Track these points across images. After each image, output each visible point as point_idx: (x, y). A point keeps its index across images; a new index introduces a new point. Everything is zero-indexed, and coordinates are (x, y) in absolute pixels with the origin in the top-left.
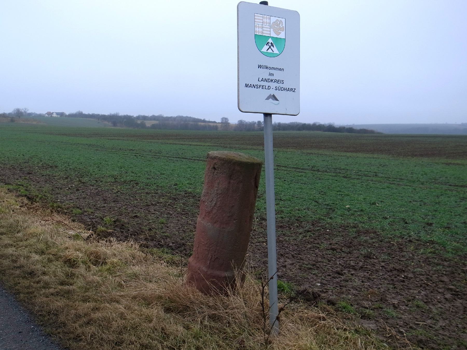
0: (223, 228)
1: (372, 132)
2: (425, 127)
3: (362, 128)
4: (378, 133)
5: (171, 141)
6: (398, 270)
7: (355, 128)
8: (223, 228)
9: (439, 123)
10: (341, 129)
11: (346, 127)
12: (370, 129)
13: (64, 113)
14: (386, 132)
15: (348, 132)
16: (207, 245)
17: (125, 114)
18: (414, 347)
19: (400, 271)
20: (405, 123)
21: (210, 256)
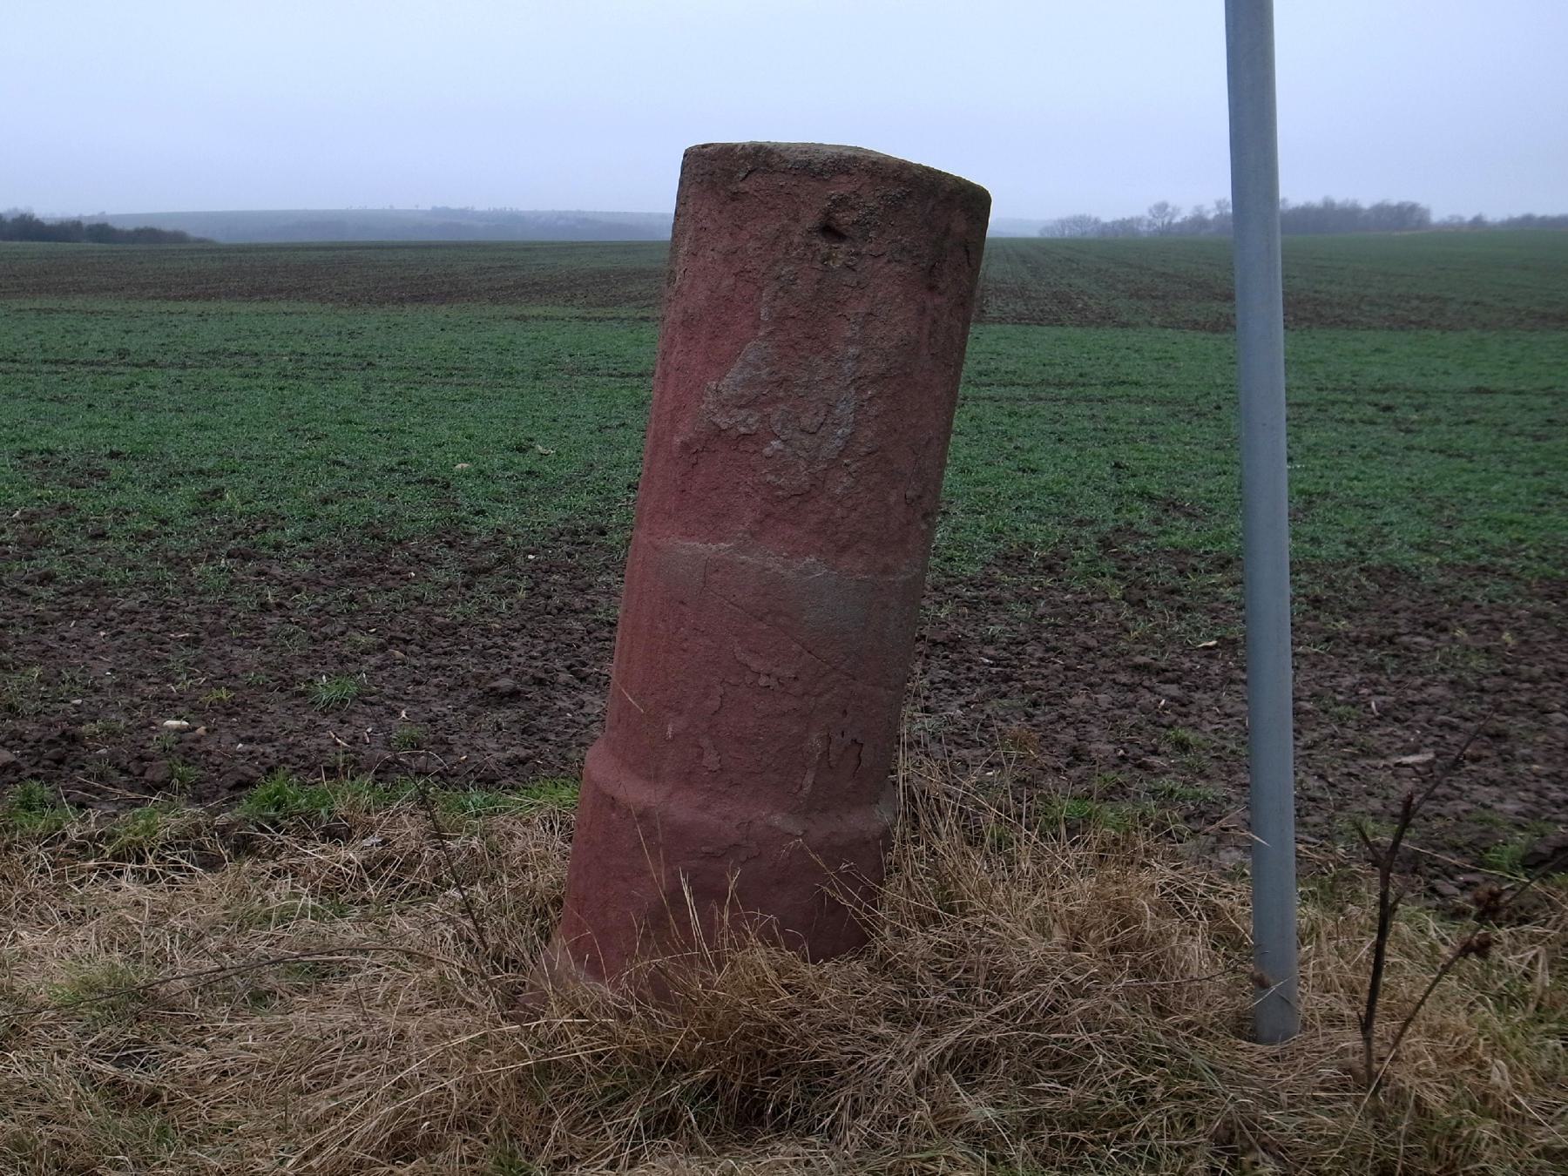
0: (886, 570)
1: (178, 237)
2: (583, 220)
3: (142, 226)
4: (200, 241)
5: (78, 302)
6: (944, 644)
7: (118, 226)
8: (886, 570)
9: (370, 207)
10: (68, 231)
11: (86, 223)
12: (168, 227)
13: (1413, 208)
14: (222, 239)
15: (94, 241)
16: (798, 687)
17: (1517, 213)
18: (1407, 765)
19: (952, 644)
20: (301, 208)
21: (815, 741)
